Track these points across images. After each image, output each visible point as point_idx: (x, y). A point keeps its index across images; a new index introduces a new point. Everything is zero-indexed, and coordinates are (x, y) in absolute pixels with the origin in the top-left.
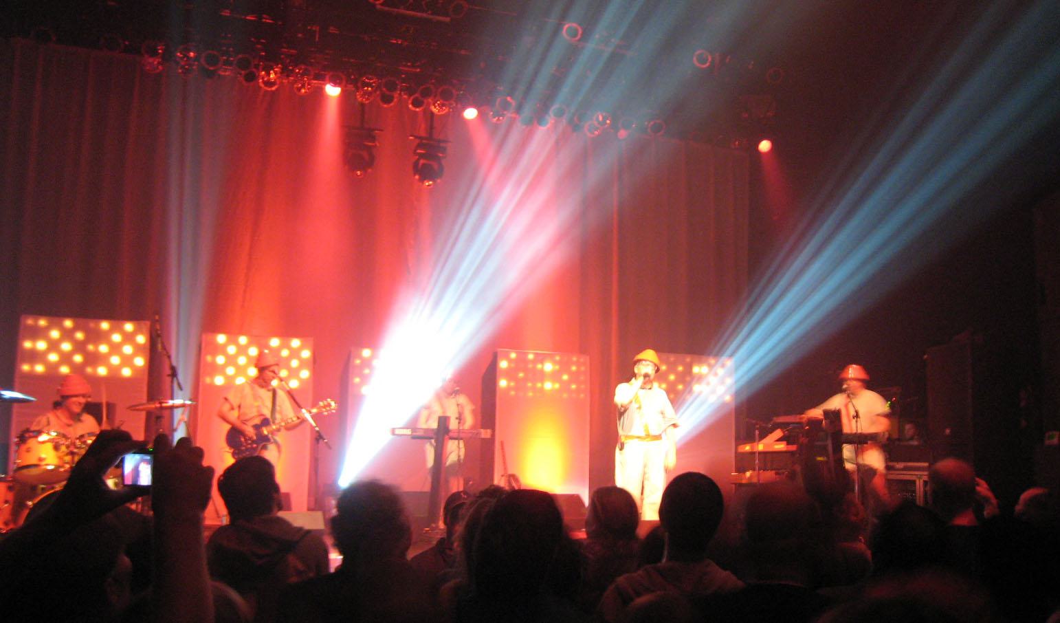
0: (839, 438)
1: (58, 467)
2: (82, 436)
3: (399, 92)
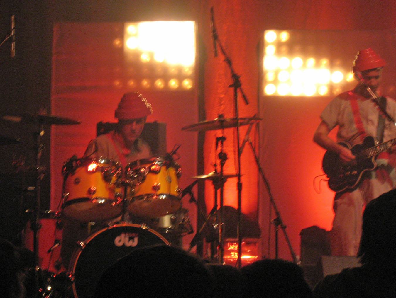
1: (108, 201)
2: (134, 164)
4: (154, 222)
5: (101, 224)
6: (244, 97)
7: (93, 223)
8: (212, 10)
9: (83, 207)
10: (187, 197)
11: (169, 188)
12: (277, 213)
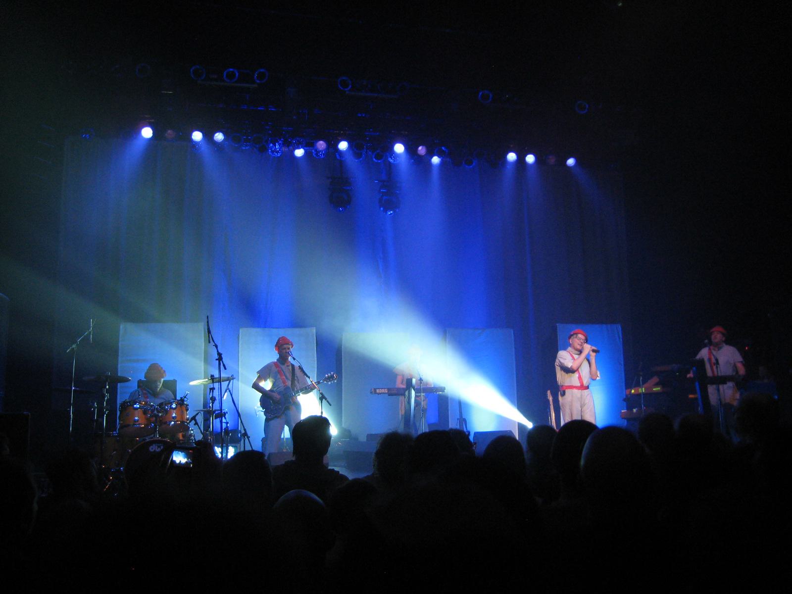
0: (704, 381)
3: (365, 150)
6: (224, 365)
8: (208, 317)
10: (193, 422)
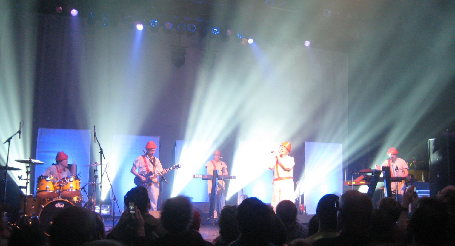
1: (54, 191)
4: (70, 199)
5: (51, 199)
7: (48, 199)
9: (44, 193)
10: (83, 190)
11: (76, 187)
12: (115, 196)
